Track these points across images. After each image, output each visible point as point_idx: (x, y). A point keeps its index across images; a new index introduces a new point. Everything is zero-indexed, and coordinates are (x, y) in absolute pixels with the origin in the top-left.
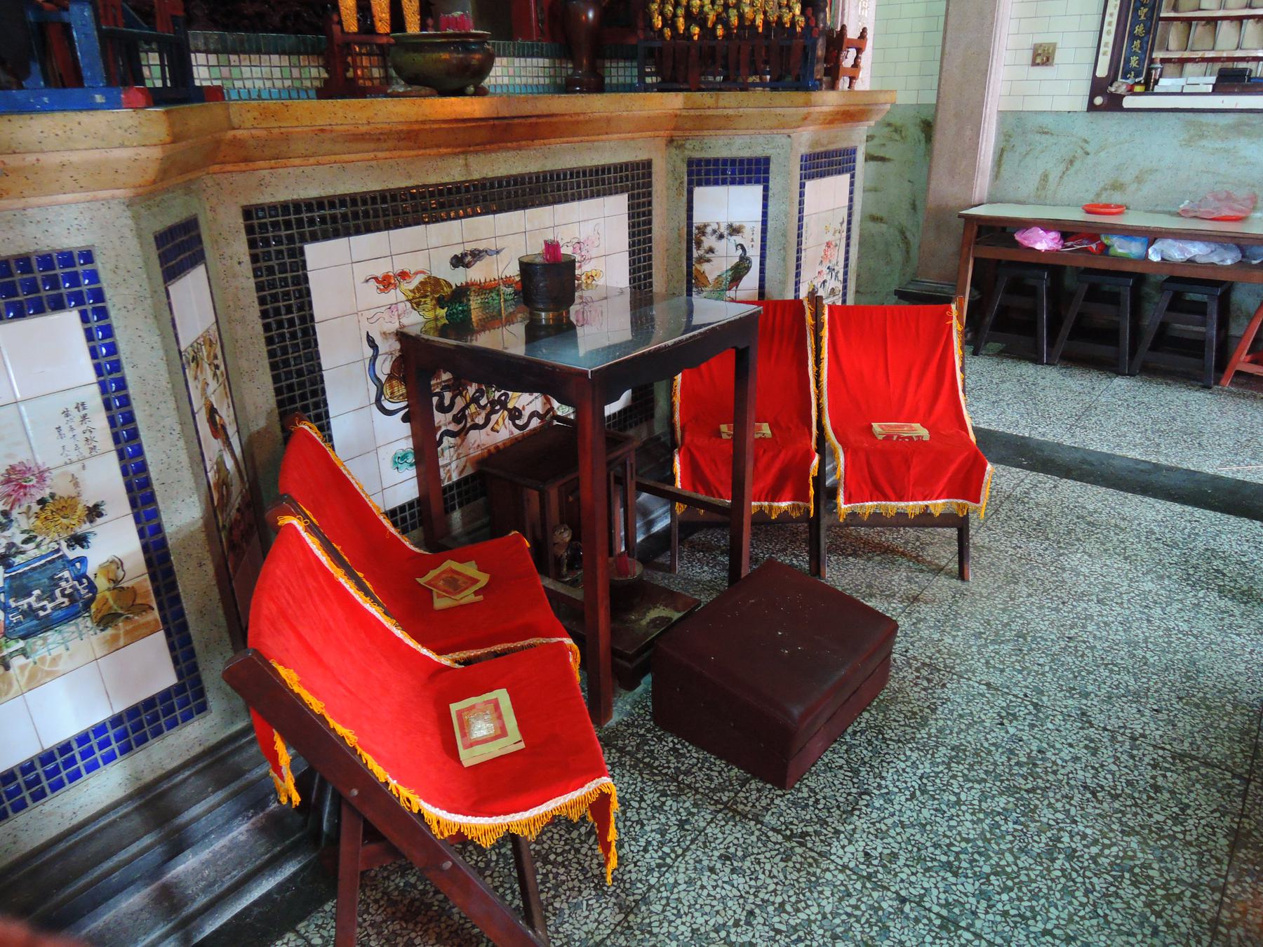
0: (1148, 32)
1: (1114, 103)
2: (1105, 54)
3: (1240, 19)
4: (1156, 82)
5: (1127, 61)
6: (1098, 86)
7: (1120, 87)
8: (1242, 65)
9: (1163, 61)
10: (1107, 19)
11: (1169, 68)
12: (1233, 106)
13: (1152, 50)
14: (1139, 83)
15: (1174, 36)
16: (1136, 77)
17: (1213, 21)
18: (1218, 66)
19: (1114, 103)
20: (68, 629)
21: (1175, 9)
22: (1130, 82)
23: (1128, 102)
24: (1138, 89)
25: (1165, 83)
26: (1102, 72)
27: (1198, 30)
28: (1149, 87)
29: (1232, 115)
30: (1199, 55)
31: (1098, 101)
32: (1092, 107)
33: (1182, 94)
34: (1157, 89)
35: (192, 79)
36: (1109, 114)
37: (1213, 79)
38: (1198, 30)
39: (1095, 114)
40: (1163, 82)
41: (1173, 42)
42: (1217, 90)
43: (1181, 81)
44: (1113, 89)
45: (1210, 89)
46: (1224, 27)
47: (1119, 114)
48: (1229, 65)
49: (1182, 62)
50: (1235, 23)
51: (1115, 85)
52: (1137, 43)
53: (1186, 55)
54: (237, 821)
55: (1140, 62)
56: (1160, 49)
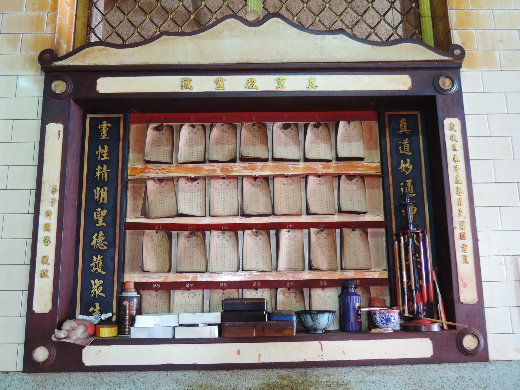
0: (111, 244)
1: (68, 359)
2: (43, 275)
3: (234, 228)
4: (132, 324)
5: (87, 287)
6: (38, 330)
7: (73, 331)
8: (250, 294)
9: (140, 287)
10: (43, 220)
11: (151, 298)
12: (253, 360)
13: (122, 271)
14: (107, 322)
15: (150, 247)
16: (102, 312)
17: (201, 230)
18: (218, 296)
19: (68, 359)
20: (159, 293)
21: (145, 213)
22: (94, 319)
23: (91, 356)
24: (106, 332)
25: (145, 324)
26: (43, 304)
27: (182, 242)
28: (122, 323)
29: (255, 373)
30: (189, 278)
31: (41, 354)
32: (30, 366)
33: (173, 341)
34: (134, 333)
35: (174, 289)
36: (63, 377)
37: (216, 317)
38: (182, 242)
39: (40, 377)
40: (141, 321)
41: (150, 261)
42: (225, 335)
43: (170, 320)
44: (61, 334)
45: (215, 332)
46: (215, 239)
47: (80, 375)
48: (234, 294)
49: (168, 287)
50: (228, 234)
51: (68, 325)
52: (98, 260)
53: (172, 278)
54: (271, 185)
55: (107, 288)
56: (133, 270)
